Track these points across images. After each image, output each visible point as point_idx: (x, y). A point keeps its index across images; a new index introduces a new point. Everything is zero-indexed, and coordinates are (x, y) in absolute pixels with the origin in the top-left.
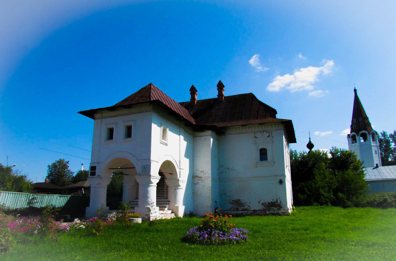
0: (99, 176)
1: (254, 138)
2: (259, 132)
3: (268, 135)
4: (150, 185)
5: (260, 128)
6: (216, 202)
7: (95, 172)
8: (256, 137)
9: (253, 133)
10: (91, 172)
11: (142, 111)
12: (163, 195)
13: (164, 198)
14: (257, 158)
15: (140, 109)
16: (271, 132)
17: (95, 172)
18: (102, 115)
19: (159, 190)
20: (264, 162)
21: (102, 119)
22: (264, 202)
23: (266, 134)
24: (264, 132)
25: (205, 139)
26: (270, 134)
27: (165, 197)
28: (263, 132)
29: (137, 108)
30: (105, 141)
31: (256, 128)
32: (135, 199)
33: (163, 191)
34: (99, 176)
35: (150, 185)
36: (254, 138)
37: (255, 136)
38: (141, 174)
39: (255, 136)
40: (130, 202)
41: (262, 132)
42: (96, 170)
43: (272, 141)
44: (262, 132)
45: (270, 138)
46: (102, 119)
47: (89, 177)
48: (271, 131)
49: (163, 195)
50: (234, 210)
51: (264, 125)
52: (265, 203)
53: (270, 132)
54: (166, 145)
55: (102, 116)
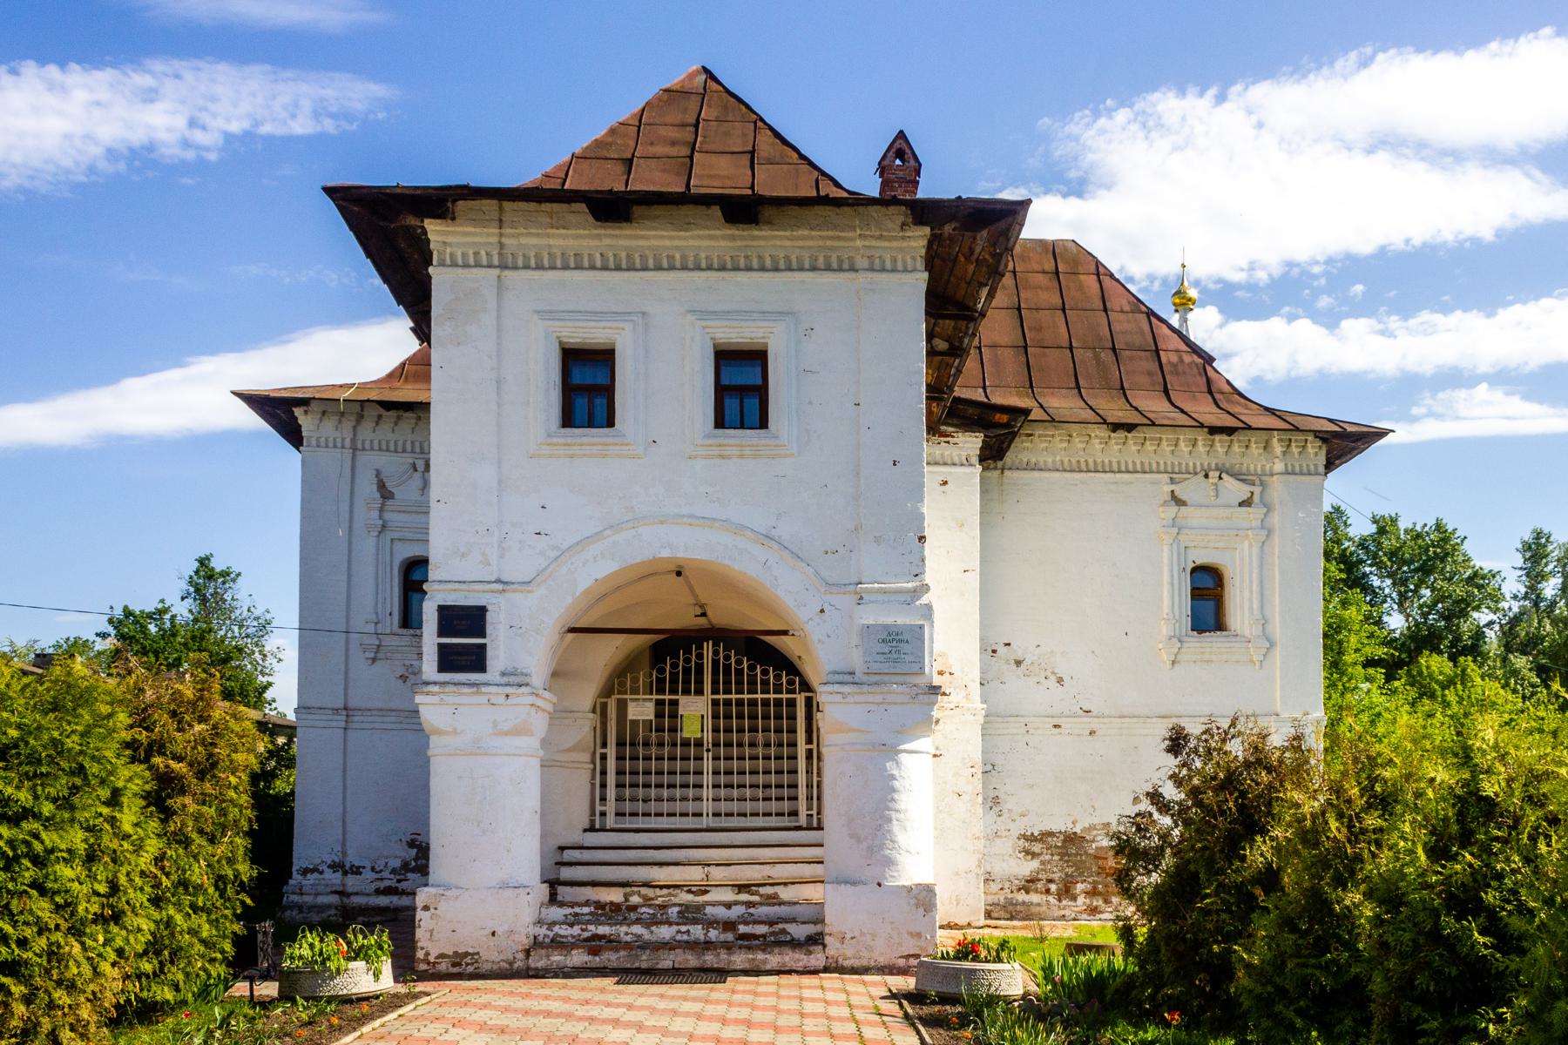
0: (512, 679)
1: (1165, 503)
2: (1196, 474)
3: (1245, 498)
4: (902, 747)
5: (1134, 448)
7: (484, 646)
8: (1179, 502)
10: (440, 645)
11: (840, 261)
12: (691, 807)
13: (689, 822)
14: (1177, 617)
15: (829, 243)
16: (1262, 483)
17: (484, 646)
18: (501, 235)
19: (670, 773)
20: (1212, 640)
21: (506, 273)
23: (1234, 489)
25: (945, 483)
26: (1252, 493)
28: (1220, 478)
29: (806, 232)
30: (549, 436)
31: (1078, 443)
32: (585, 831)
33: (692, 779)
34: (512, 679)
35: (902, 747)
36: (1165, 503)
37: (1172, 491)
38: (859, 677)
39: (1172, 491)
40: (562, 849)
41: (1214, 475)
42: (489, 629)
43: (1262, 527)
44: (1211, 474)
45: (1255, 513)
46: (504, 267)
47: (427, 683)
48: (1264, 478)
49: (691, 807)
50: (1048, 891)
53: (1257, 482)
55: (502, 245)
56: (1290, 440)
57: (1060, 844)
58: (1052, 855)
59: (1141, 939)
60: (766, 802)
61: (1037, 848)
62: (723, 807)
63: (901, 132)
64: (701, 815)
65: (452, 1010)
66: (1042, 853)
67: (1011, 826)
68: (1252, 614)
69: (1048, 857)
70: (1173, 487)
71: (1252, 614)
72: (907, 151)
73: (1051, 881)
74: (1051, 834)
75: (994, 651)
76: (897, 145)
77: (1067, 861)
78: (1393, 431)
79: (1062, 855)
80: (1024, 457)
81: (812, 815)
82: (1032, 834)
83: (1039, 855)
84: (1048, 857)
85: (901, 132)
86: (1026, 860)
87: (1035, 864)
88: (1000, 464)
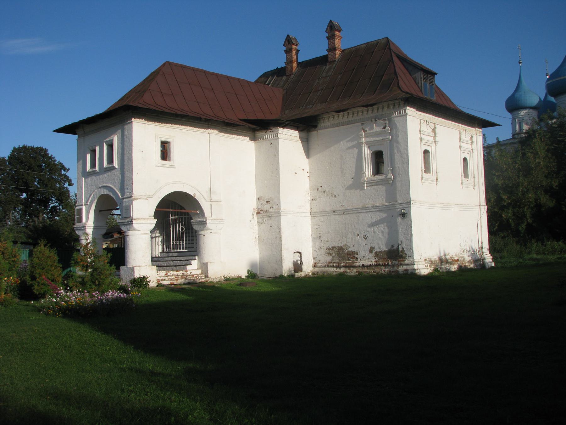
6: (300, 253)
7: (81, 217)
9: (360, 124)
17: (81, 217)
22: (378, 250)
24: (376, 120)
27: (195, 248)
28: (376, 121)
41: (373, 120)
51: (341, 113)
52: (381, 252)
54: (173, 167)
56: (348, 113)
57: (337, 251)
58: (335, 254)
59: (91, 269)
60: (192, 244)
61: (331, 252)
62: (188, 246)
63: (330, 20)
64: (193, 248)
65: (175, 274)
66: (333, 254)
67: (325, 245)
68: (162, 280)
69: (334, 255)
70: (362, 127)
71: (162, 280)
72: (333, 26)
73: (334, 263)
74: (335, 247)
75: (318, 189)
76: (330, 25)
77: (340, 256)
78: (501, 125)
79: (338, 254)
80: (323, 125)
81: (169, 279)
82: (330, 247)
83: (332, 254)
84: (334, 255)
85: (330, 20)
86: (329, 256)
87: (331, 257)
88: (317, 129)
